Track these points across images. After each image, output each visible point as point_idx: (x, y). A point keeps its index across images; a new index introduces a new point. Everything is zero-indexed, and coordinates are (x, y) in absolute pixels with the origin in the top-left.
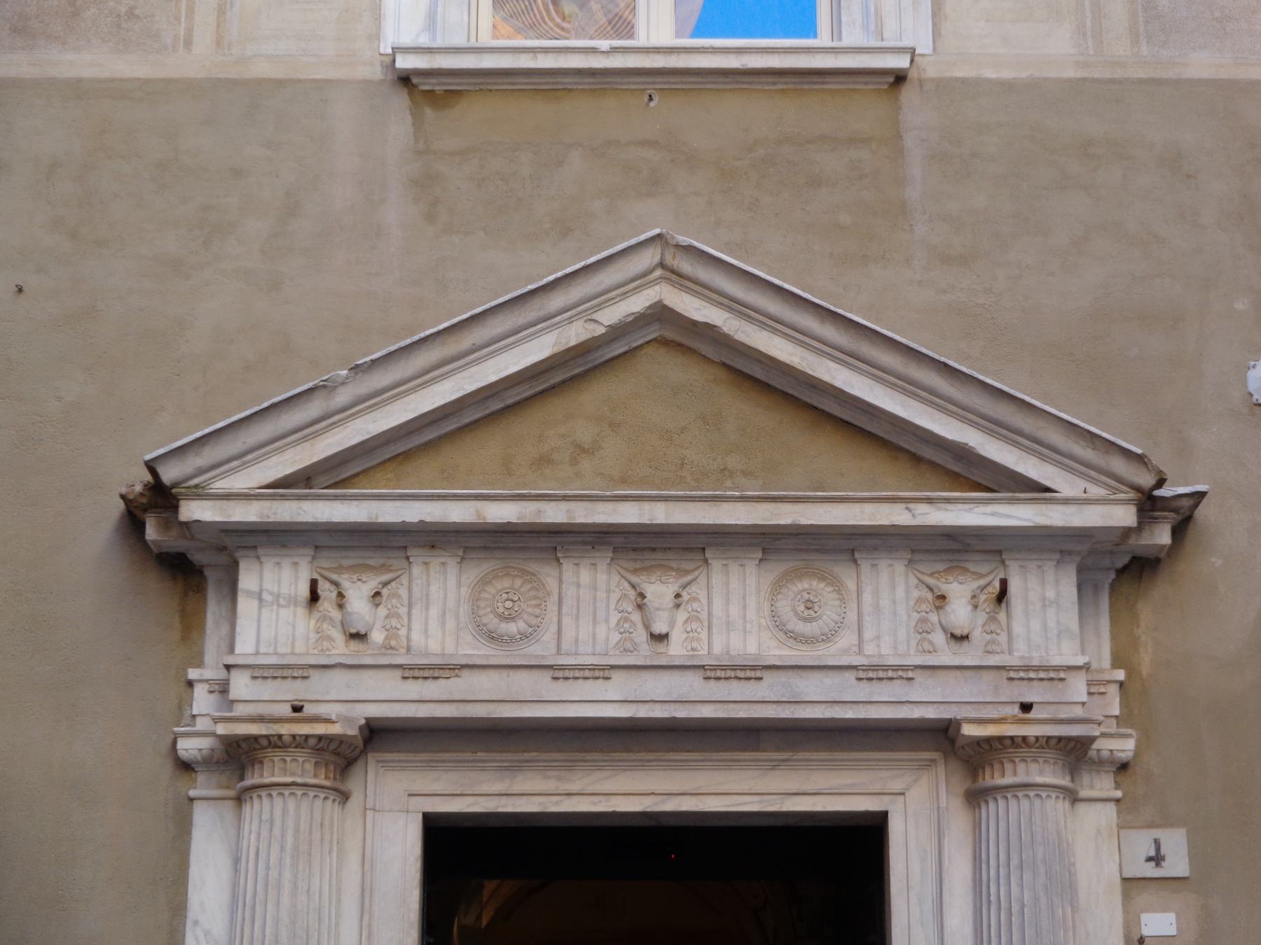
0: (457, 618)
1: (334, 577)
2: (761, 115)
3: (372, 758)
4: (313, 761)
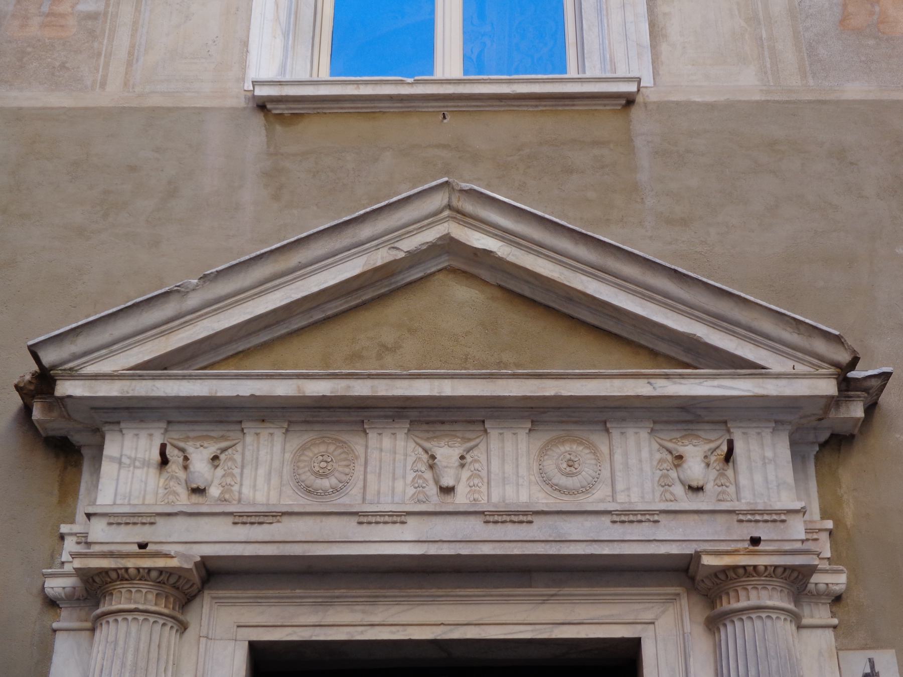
0: (281, 477)
1: (182, 444)
2: (525, 128)
3: (207, 595)
4: (155, 592)
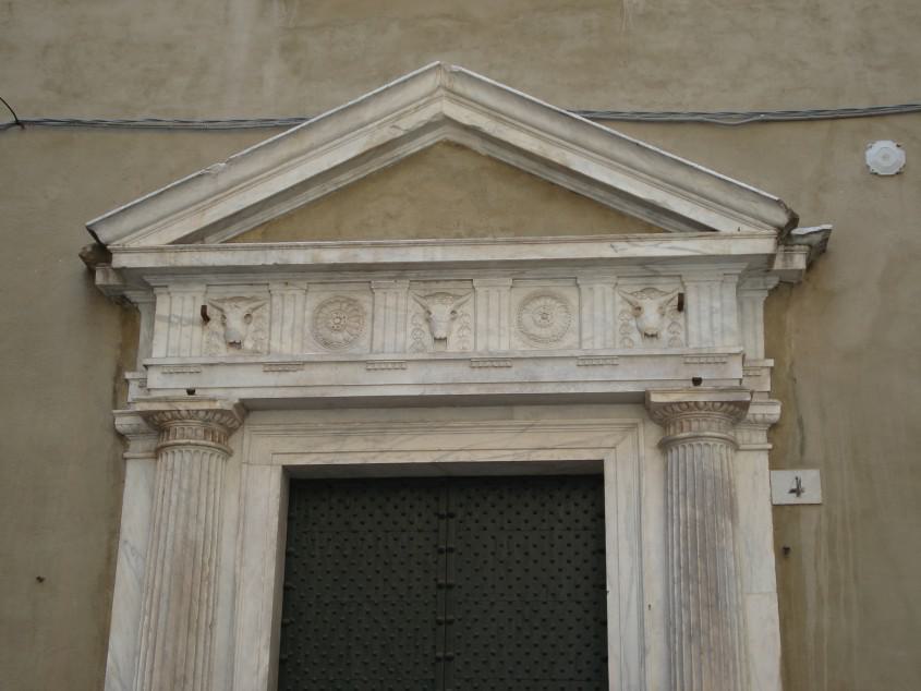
0: (303, 331)
1: (220, 305)
